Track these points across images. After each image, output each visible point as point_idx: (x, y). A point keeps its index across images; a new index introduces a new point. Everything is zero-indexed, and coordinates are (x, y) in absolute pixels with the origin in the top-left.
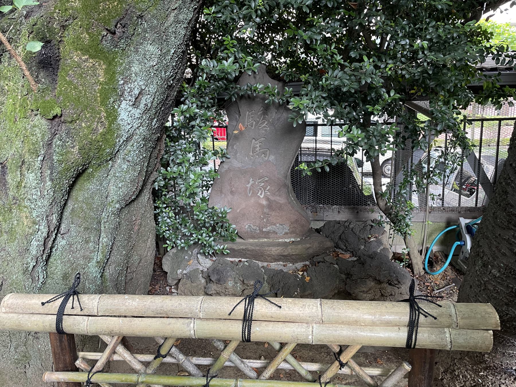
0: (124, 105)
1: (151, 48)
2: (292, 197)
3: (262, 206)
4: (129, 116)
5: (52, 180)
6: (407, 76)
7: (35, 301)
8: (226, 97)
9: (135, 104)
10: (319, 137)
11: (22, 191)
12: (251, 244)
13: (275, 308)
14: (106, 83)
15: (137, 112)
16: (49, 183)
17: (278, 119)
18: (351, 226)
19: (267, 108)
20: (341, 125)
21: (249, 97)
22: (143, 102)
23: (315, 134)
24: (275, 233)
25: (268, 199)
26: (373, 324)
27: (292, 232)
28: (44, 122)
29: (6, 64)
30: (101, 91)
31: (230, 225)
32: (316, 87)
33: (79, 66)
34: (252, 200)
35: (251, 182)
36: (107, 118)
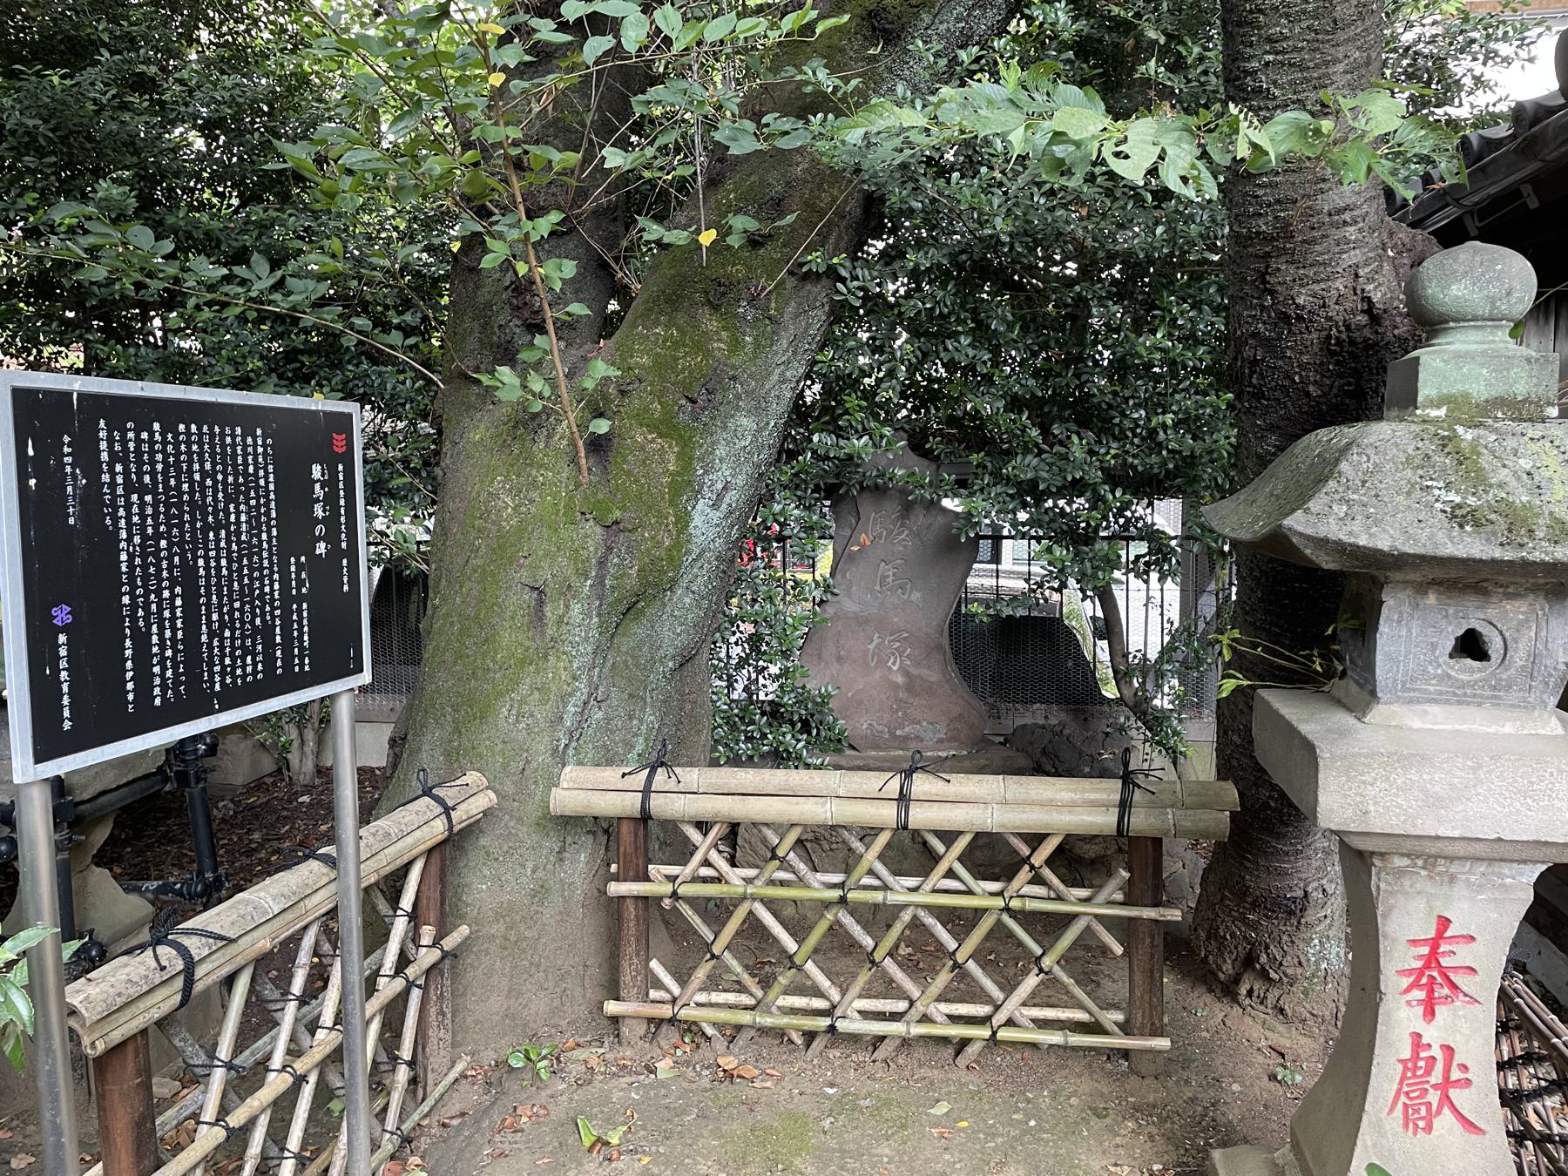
1: (744, 421)
2: (953, 673)
3: (896, 686)
4: (706, 523)
5: (599, 615)
6: (1140, 468)
7: (611, 775)
8: (839, 488)
9: (715, 506)
10: (1006, 564)
11: (564, 629)
12: (872, 758)
13: (941, 784)
15: (715, 516)
16: (596, 620)
17: (928, 527)
18: (1066, 732)
19: (908, 508)
20: (1039, 539)
21: (876, 486)
22: (727, 500)
23: (996, 558)
24: (919, 739)
25: (906, 674)
26: (1073, 805)
27: (952, 739)
28: (598, 530)
29: (542, 445)
30: (670, 485)
31: (835, 720)
32: (998, 477)
33: (643, 449)
34: (877, 675)
35: (876, 641)
36: (675, 524)
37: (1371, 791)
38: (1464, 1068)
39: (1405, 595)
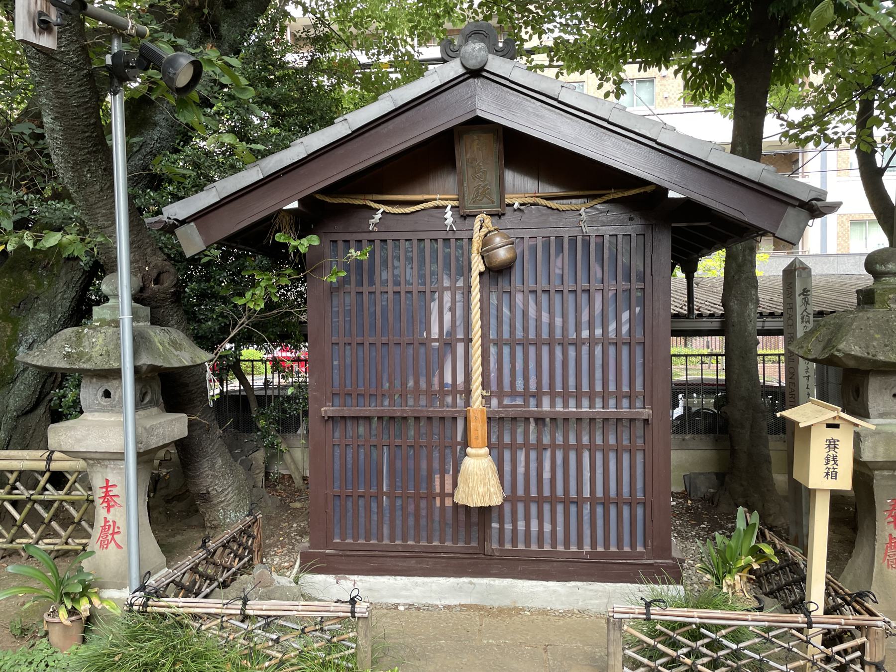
0: (21, 349)
1: (43, 315)
14: (11, 336)
37: (62, 438)
38: (118, 528)
39: (87, 379)
